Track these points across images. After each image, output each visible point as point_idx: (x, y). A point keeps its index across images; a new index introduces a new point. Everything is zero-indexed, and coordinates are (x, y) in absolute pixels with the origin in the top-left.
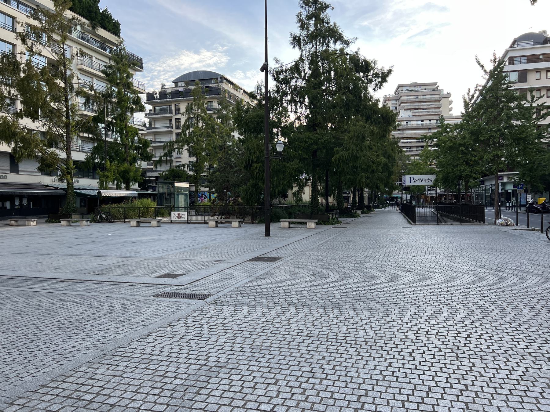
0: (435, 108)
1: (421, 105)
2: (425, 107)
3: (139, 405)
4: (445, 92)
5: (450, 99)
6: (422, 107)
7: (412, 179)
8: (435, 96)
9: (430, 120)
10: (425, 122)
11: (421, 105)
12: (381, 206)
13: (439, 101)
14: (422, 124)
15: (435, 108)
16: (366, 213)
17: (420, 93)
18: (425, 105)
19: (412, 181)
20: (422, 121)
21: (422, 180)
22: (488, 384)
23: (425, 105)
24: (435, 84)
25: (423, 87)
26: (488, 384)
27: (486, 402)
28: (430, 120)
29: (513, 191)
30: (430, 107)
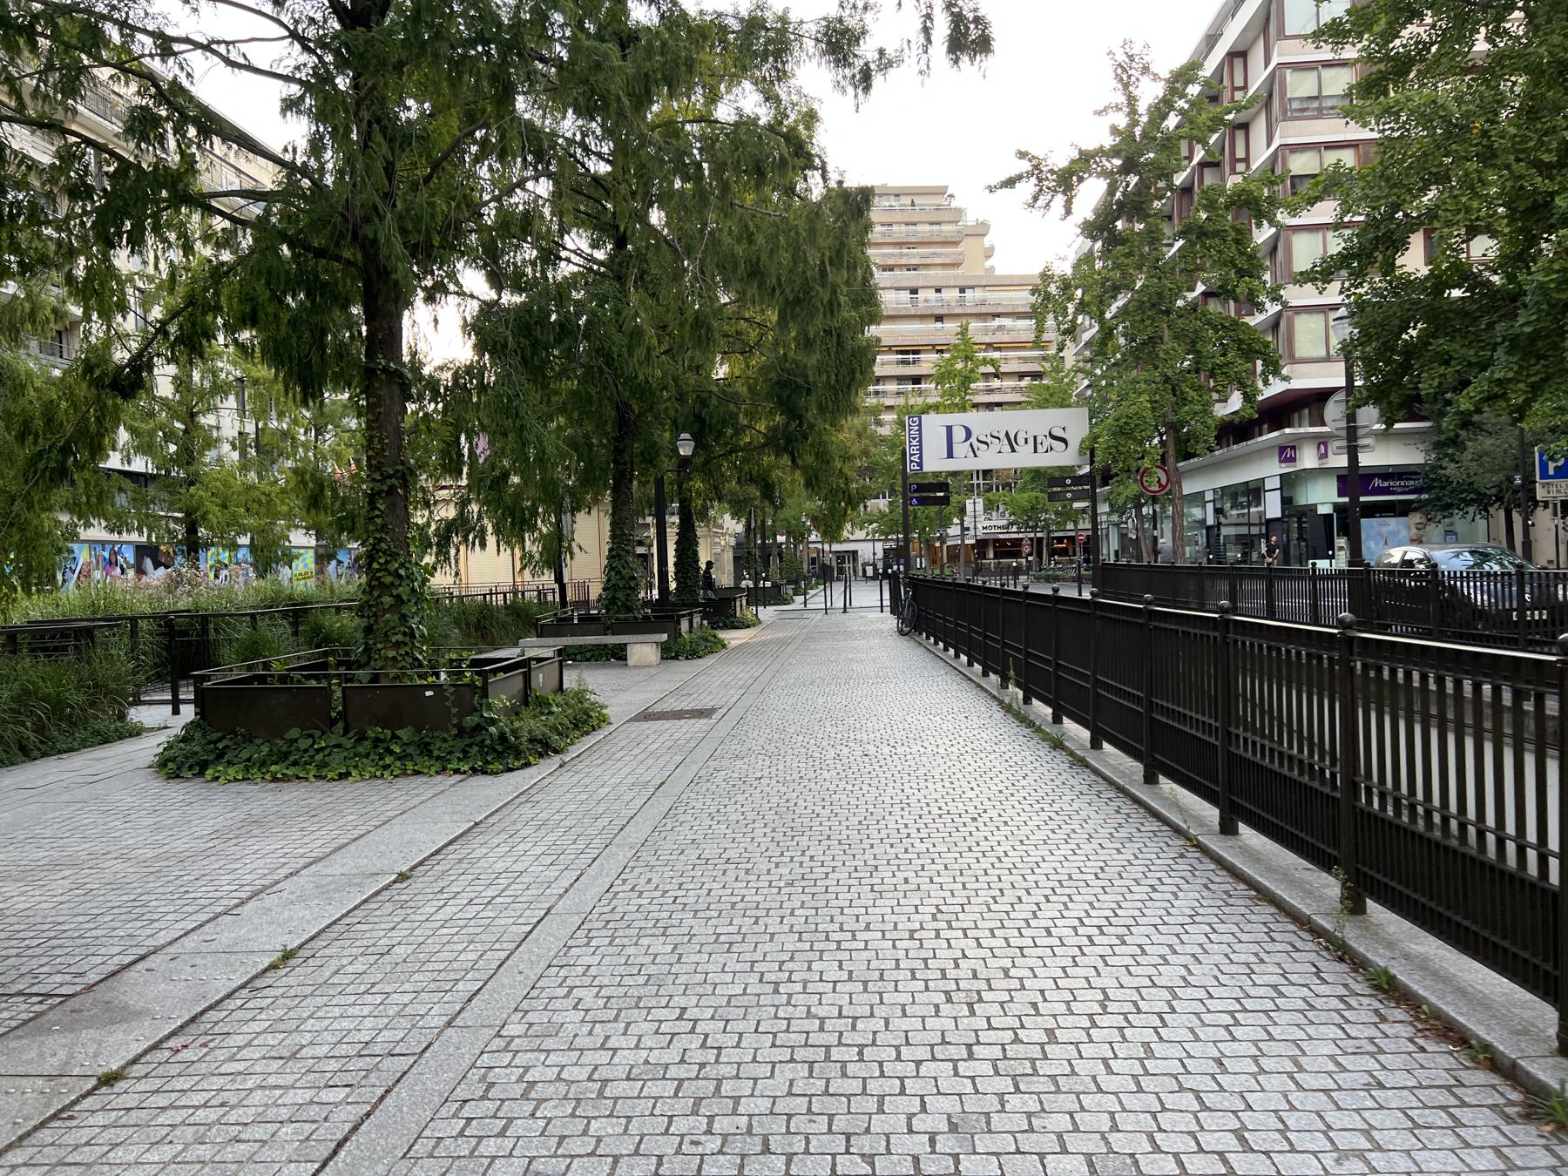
0: (944, 265)
1: (902, 255)
2: (915, 261)
3: (111, 1154)
4: (971, 218)
5: (987, 241)
6: (904, 261)
7: (959, 434)
8: (944, 227)
9: (938, 291)
10: (922, 295)
11: (902, 255)
12: (790, 589)
13: (956, 243)
14: (914, 302)
15: (944, 265)
16: (693, 654)
17: (899, 217)
18: (914, 255)
19: (960, 449)
20: (914, 291)
21: (1012, 443)
22: (1138, 1084)
23: (914, 255)
24: (940, 191)
25: (907, 200)
26: (1138, 1084)
27: (1063, 1008)
28: (938, 291)
29: (1336, 506)
30: (928, 261)
